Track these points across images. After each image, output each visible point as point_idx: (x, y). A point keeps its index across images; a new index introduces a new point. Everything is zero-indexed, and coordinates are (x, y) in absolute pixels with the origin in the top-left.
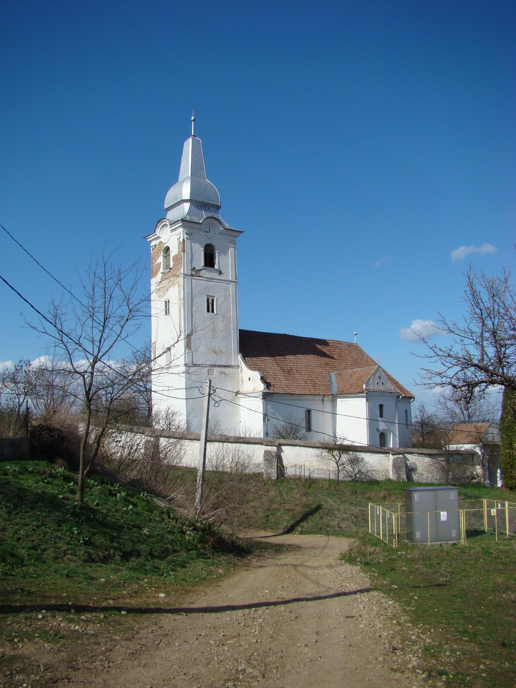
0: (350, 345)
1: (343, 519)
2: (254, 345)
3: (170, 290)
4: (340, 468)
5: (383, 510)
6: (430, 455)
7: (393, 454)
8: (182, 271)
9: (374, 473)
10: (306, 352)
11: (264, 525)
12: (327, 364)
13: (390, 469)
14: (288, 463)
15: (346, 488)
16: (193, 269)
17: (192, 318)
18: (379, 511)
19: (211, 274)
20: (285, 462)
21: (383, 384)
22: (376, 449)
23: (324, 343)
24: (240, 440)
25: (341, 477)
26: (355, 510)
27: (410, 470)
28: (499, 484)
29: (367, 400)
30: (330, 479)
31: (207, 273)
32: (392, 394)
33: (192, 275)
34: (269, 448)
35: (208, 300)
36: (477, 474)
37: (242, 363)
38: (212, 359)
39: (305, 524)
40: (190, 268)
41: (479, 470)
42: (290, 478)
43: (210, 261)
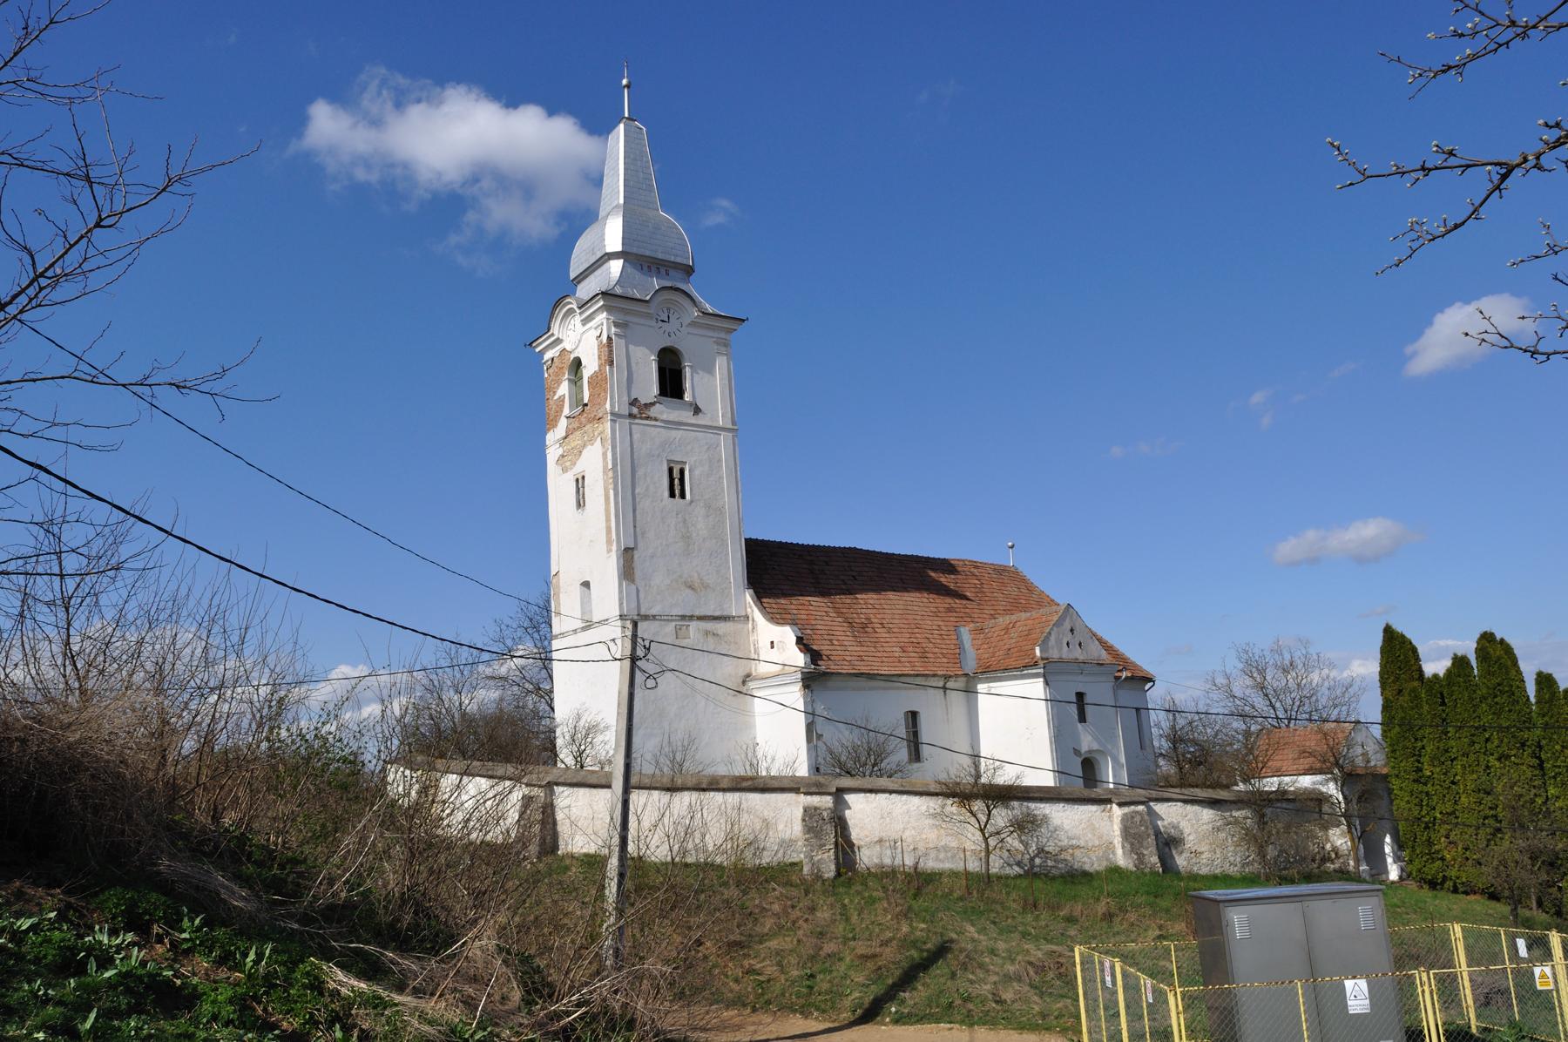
0: (1001, 570)
1: (1008, 979)
2: (777, 571)
3: (585, 452)
4: (992, 842)
5: (1125, 975)
6: (1213, 803)
7: (1120, 805)
8: (608, 406)
10: (902, 585)
11: (802, 1001)
12: (949, 610)
13: (1117, 841)
14: (862, 835)
15: (1008, 894)
16: (634, 402)
17: (634, 511)
18: (1113, 976)
20: (856, 835)
22: (1077, 795)
23: (946, 566)
24: (745, 784)
25: (996, 866)
26: (1037, 953)
27: (1168, 843)
28: (1394, 874)
29: (1047, 683)
30: (967, 873)
31: (666, 411)
33: (631, 416)
34: (815, 800)
35: (671, 470)
36: (1335, 850)
39: (907, 995)
40: (625, 399)
41: (1339, 838)
42: (870, 873)
43: (671, 384)
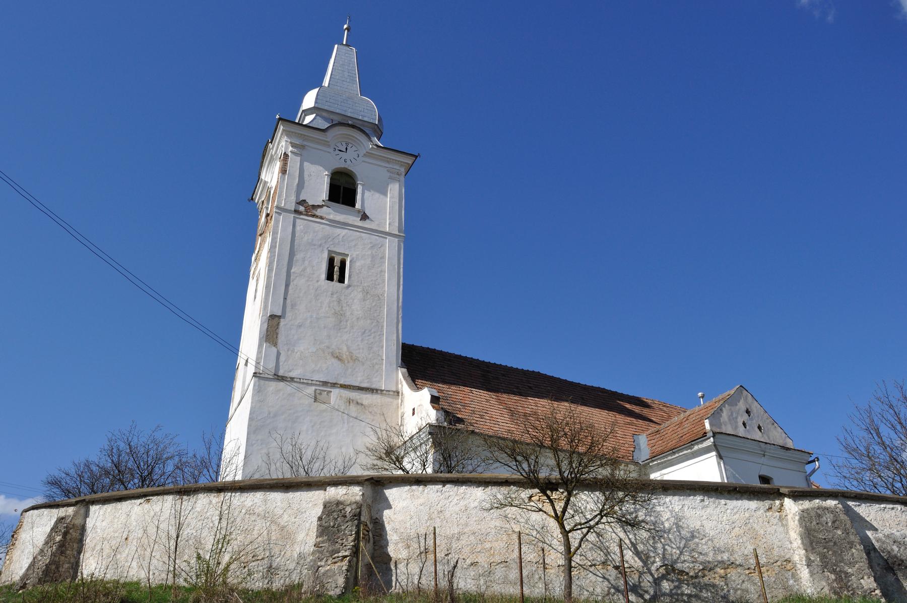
9: (733, 573)
13: (798, 555)
17: (287, 286)
19: (344, 216)
21: (759, 428)
29: (720, 457)
31: (335, 213)
32: (788, 453)
33: (296, 212)
35: (331, 261)
37: (404, 383)
38: (329, 370)
40: (293, 198)
